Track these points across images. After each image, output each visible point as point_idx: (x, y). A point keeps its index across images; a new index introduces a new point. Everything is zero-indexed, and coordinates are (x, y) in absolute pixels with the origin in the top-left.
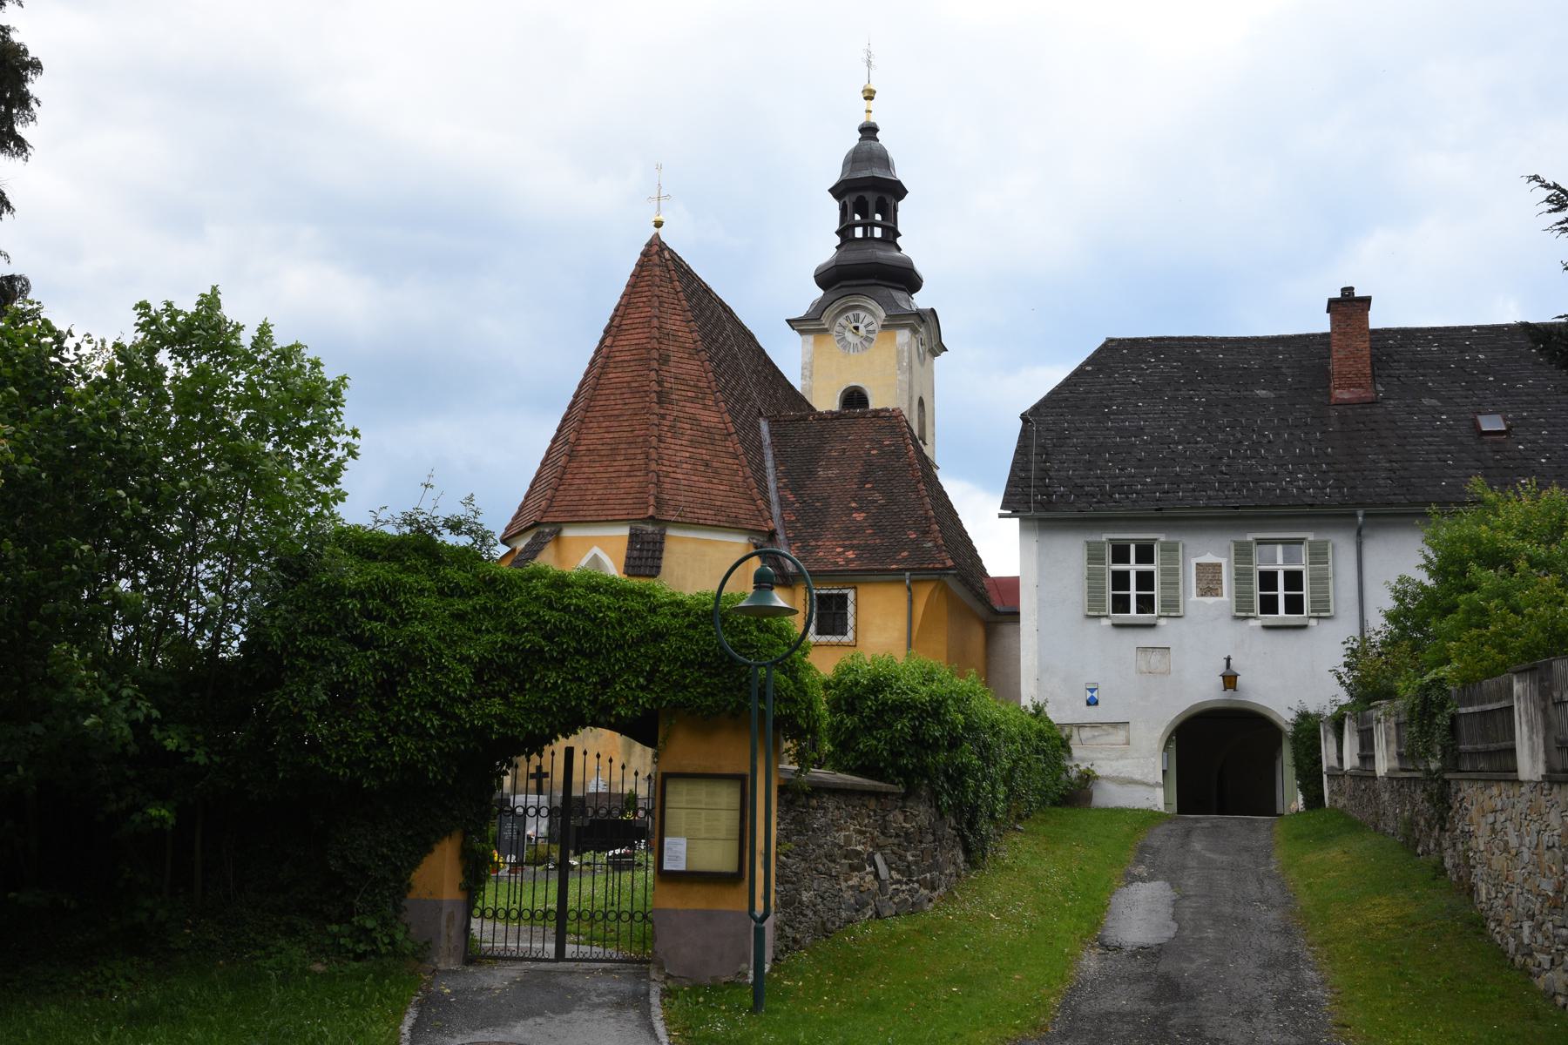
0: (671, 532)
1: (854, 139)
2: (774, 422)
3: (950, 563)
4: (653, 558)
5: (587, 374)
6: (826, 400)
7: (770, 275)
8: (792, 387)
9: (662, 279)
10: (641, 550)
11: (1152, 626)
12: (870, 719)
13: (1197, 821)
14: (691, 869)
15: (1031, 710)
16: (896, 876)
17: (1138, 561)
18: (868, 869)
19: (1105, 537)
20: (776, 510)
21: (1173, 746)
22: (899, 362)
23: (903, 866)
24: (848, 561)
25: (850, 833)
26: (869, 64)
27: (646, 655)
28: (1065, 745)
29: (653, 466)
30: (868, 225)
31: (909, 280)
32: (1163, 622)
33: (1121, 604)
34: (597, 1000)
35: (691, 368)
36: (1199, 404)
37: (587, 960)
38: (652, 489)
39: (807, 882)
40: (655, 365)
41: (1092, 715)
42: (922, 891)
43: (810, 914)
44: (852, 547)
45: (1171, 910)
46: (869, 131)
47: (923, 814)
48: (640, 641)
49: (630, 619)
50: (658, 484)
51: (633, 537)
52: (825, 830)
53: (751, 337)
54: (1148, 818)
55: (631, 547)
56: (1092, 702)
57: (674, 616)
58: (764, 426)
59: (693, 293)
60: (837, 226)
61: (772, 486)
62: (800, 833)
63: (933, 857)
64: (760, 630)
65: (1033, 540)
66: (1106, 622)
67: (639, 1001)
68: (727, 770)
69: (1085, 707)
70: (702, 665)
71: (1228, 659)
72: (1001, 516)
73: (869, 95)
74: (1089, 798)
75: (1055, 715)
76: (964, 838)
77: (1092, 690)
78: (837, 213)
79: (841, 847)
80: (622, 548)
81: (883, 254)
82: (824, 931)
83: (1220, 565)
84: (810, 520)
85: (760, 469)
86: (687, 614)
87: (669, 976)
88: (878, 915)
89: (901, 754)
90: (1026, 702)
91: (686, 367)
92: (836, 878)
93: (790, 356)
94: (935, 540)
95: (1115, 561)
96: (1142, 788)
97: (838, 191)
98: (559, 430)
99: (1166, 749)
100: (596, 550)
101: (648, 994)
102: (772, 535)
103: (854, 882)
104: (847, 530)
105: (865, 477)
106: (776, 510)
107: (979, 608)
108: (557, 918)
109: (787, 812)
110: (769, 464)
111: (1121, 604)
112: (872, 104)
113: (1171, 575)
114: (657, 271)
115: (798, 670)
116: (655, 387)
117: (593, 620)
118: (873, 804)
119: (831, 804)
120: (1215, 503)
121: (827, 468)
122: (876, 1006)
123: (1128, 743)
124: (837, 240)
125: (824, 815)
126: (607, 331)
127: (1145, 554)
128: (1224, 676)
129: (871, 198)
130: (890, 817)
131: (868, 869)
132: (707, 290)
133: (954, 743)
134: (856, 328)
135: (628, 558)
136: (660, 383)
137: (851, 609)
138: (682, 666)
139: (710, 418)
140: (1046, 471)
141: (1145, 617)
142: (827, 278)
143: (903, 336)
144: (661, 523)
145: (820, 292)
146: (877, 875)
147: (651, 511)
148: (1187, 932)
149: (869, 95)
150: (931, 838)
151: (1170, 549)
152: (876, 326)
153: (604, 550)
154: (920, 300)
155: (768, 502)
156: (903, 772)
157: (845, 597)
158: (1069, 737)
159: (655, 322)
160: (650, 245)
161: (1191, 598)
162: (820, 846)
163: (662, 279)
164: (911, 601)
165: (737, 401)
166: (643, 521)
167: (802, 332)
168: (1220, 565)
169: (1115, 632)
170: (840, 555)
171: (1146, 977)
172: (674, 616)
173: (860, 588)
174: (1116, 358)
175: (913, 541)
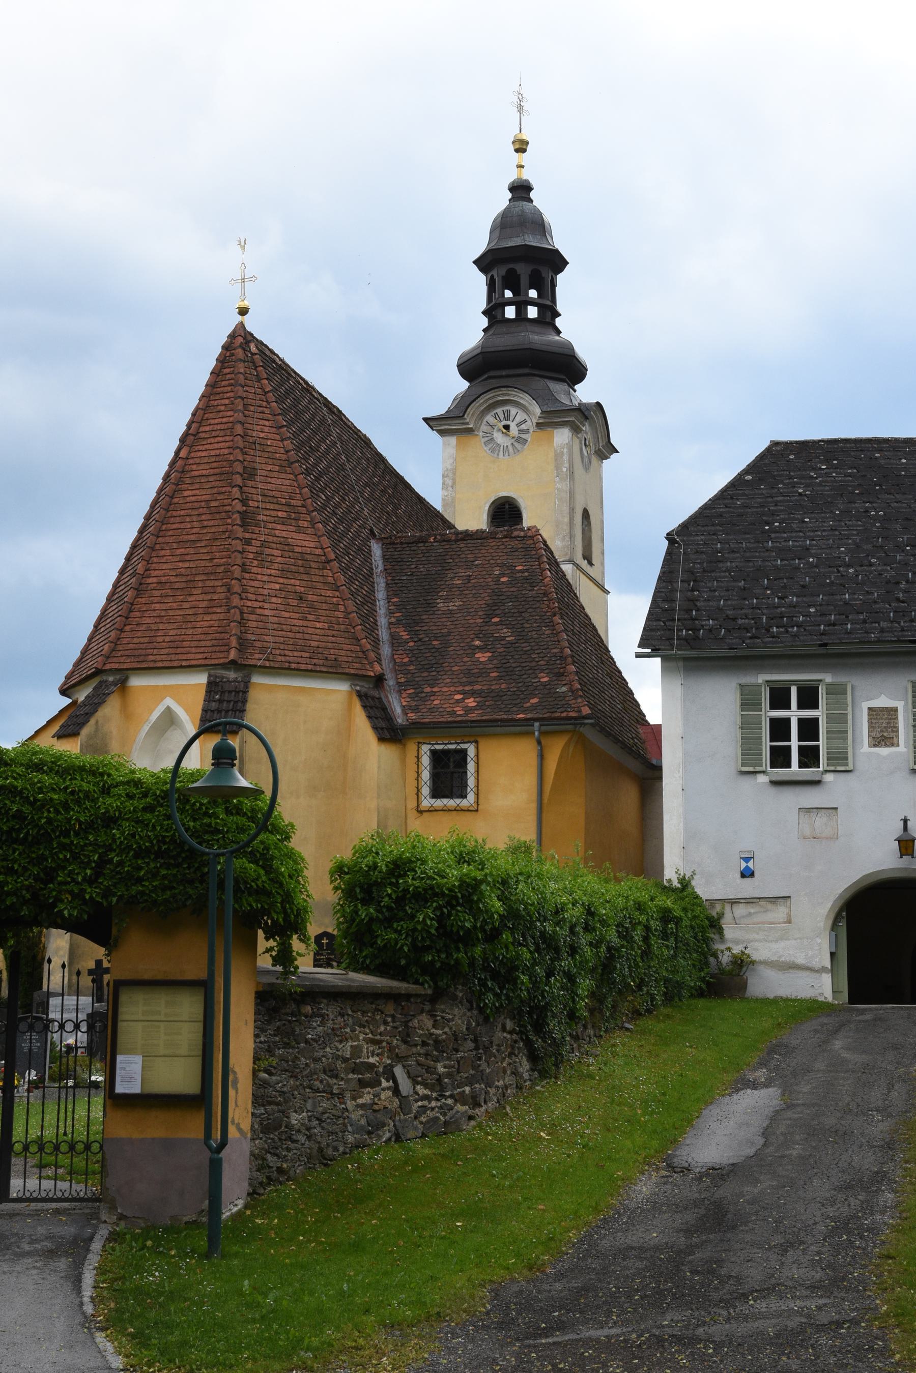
0: (256, 679)
1: (503, 199)
2: (388, 544)
3: (586, 711)
4: (234, 710)
5: (160, 491)
6: (471, 517)
7: (393, 370)
8: (421, 500)
9: (248, 372)
10: (220, 701)
11: (817, 783)
12: (389, 908)
13: (863, 1012)
14: (147, 1091)
15: (676, 884)
16: (421, 1090)
17: (800, 706)
18: (384, 1084)
19: (761, 678)
20: (386, 650)
21: (843, 924)
22: (558, 468)
23: (431, 1079)
24: (469, 710)
25: (361, 1043)
26: (520, 109)
27: (95, 844)
28: (715, 924)
29: (236, 601)
30: (521, 305)
31: (571, 369)
32: (829, 778)
33: (780, 758)
34: (27, 1248)
35: (282, 483)
36: (876, 518)
37: (36, 1200)
38: (235, 629)
39: (297, 1102)
40: (238, 480)
41: (747, 888)
42: (459, 1108)
43: (302, 1138)
44: (473, 694)
45: (767, 1123)
46: (521, 190)
47: (458, 1018)
48: (89, 826)
49: (78, 802)
50: (242, 623)
51: (212, 686)
52: (323, 1041)
53: (367, 442)
54: (814, 1007)
55: (208, 698)
56: (747, 874)
57: (130, 797)
58: (377, 550)
59: (287, 393)
60: (483, 305)
61: (383, 621)
62: (287, 1045)
63: (476, 1067)
64: (228, 812)
65: (677, 685)
66: (762, 779)
67: (77, 1249)
68: (190, 976)
69: (739, 880)
70: (159, 854)
71: (905, 821)
72: (638, 655)
73: (521, 147)
74: (743, 986)
75: (703, 890)
76: (529, 1043)
77: (747, 860)
78: (484, 289)
79: (345, 1060)
80: (198, 700)
81: (539, 339)
82: (324, 1159)
83: (896, 710)
84: (425, 661)
85: (369, 601)
86: (145, 795)
87: (122, 1217)
88: (398, 1137)
89: (427, 949)
90: (670, 874)
91: (275, 482)
92: (341, 1096)
93: (425, 466)
94: (570, 683)
95: (773, 706)
96: (805, 974)
97: (484, 263)
98: (128, 559)
99: (834, 926)
100: (169, 702)
101: (91, 1239)
102: (379, 680)
103: (366, 1099)
104: (468, 673)
105: (492, 609)
106: (386, 650)
107: (632, 764)
108: (11, 1146)
109: (269, 1022)
110: (381, 594)
111: (780, 758)
112: (524, 158)
113: (839, 721)
114: (241, 367)
115: (273, 858)
116: (239, 506)
117: (32, 804)
118: (390, 1008)
119: (331, 1011)
120: (888, 636)
121: (447, 599)
122: (357, 1247)
123: (789, 921)
124: (484, 322)
125: (323, 1024)
126: (183, 440)
127: (809, 698)
128: (899, 841)
129: (523, 270)
130: (415, 1023)
131: (384, 1084)
132: (308, 389)
133: (493, 936)
134: (507, 427)
135: (205, 711)
136: (244, 502)
137: (471, 767)
138: (137, 856)
139: (305, 542)
140: (693, 601)
141: (809, 773)
142: (473, 367)
143: (562, 436)
144: (246, 669)
145: (464, 385)
146: (396, 1091)
147: (233, 655)
148: (771, 1149)
149: (521, 147)
150: (471, 1045)
151: (838, 691)
152: (529, 425)
153: (179, 702)
154: (585, 393)
155: (376, 642)
156: (427, 969)
157: (464, 752)
158: (721, 915)
159: (239, 429)
160: (232, 336)
161: (863, 749)
162: (316, 1060)
163: (248, 372)
164: (541, 757)
165: (341, 520)
166: (224, 666)
167: (442, 433)
168: (896, 710)
169: (773, 790)
170: (459, 703)
171: (696, 1204)
172: (130, 797)
173: (483, 743)
174: (782, 466)
175: (544, 685)
